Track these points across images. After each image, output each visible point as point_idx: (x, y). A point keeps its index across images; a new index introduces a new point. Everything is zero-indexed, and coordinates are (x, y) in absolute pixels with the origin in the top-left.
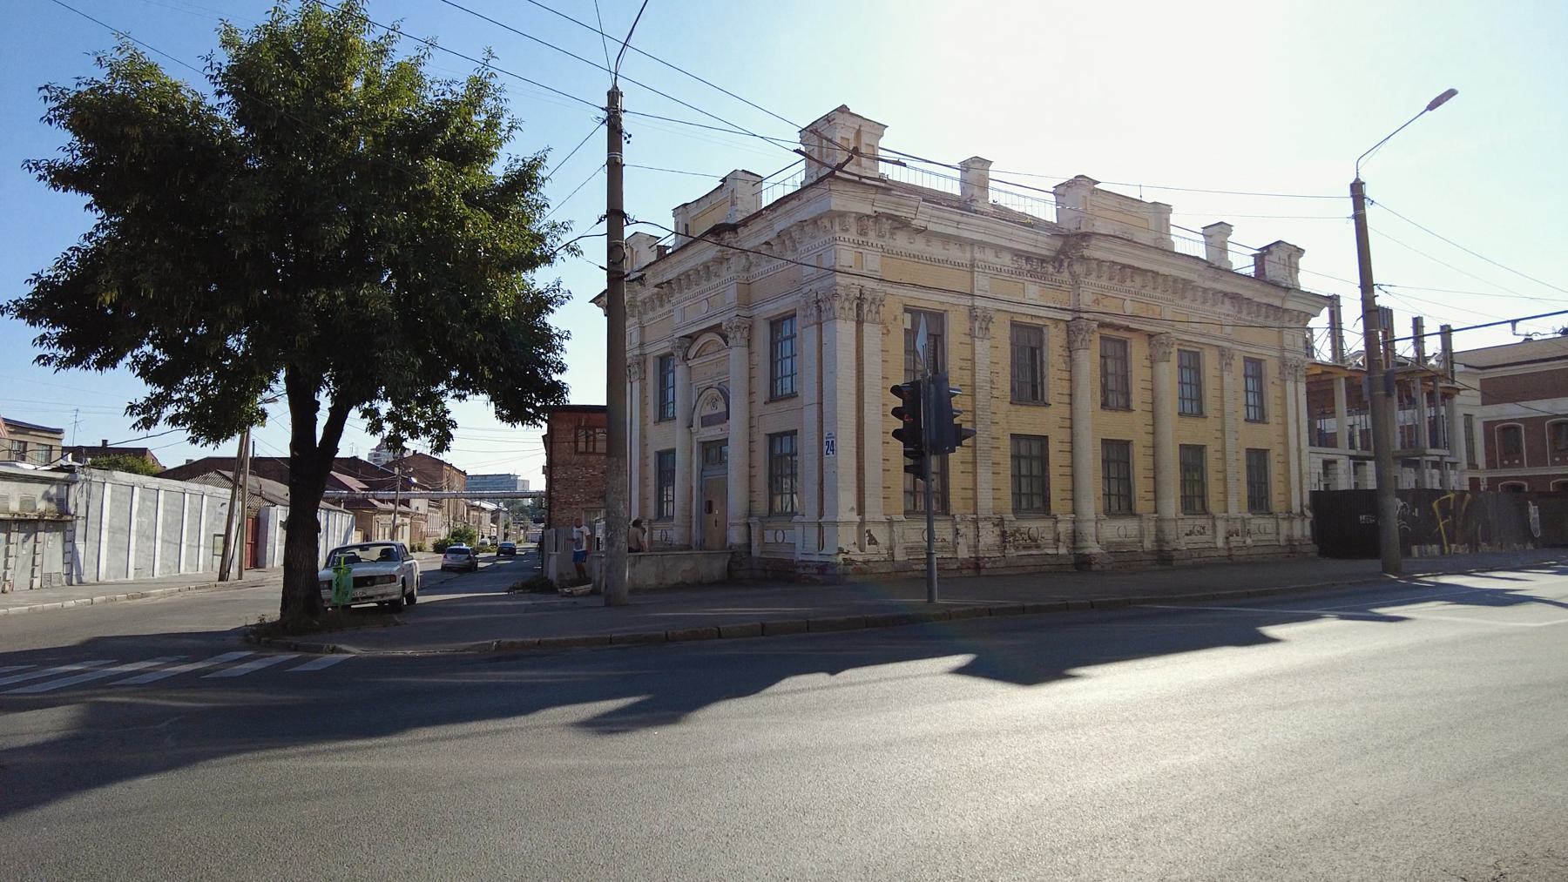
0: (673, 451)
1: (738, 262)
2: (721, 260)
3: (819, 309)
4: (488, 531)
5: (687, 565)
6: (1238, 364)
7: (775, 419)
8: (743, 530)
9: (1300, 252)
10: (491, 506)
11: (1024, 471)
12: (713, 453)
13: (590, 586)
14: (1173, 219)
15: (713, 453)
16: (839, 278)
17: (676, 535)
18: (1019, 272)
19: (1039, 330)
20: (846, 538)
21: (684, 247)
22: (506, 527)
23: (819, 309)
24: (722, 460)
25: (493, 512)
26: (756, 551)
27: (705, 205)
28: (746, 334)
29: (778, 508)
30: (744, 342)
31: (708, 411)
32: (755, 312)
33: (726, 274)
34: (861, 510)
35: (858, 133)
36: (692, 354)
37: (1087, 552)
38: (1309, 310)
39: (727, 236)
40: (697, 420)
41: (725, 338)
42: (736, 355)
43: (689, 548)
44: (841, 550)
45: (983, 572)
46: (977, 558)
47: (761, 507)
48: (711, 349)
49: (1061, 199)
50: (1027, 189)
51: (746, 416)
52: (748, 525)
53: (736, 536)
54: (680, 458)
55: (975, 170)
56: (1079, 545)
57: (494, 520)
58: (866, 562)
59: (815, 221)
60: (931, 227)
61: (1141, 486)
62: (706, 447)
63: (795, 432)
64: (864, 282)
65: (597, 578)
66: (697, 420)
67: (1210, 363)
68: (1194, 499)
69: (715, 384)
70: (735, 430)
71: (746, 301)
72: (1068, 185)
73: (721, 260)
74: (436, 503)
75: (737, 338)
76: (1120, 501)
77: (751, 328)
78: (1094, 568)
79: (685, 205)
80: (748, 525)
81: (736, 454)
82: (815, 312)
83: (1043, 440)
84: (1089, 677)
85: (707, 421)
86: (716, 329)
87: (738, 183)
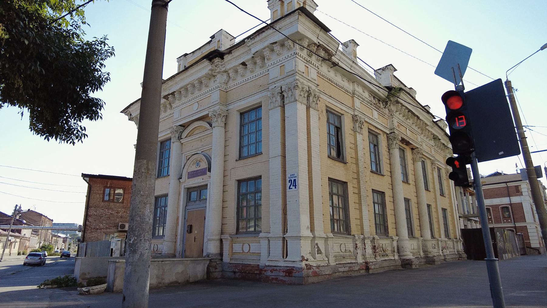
0: (166, 196)
1: (221, 78)
2: (211, 76)
3: (283, 97)
4: (59, 246)
5: (180, 268)
7: (247, 169)
8: (218, 243)
10: (64, 236)
12: (195, 195)
13: (104, 286)
15: (194, 195)
17: (165, 247)
20: (305, 248)
22: (70, 245)
23: (283, 97)
24: (201, 199)
25: (64, 238)
26: (226, 258)
28: (224, 120)
31: (194, 168)
32: (230, 107)
33: (212, 84)
36: (184, 135)
37: (408, 257)
39: (217, 60)
42: (218, 132)
43: (174, 256)
44: (303, 259)
45: (371, 272)
46: (367, 263)
47: (231, 227)
51: (222, 171)
52: (221, 241)
53: (212, 248)
54: (171, 201)
56: (402, 254)
57: (64, 241)
58: (318, 267)
60: (340, 64)
62: (189, 190)
65: (111, 279)
71: (225, 101)
73: (211, 76)
74: (35, 232)
75: (218, 123)
77: (227, 117)
78: (414, 267)
79: (186, 55)
80: (221, 241)
81: (213, 195)
82: (279, 98)
85: (193, 175)
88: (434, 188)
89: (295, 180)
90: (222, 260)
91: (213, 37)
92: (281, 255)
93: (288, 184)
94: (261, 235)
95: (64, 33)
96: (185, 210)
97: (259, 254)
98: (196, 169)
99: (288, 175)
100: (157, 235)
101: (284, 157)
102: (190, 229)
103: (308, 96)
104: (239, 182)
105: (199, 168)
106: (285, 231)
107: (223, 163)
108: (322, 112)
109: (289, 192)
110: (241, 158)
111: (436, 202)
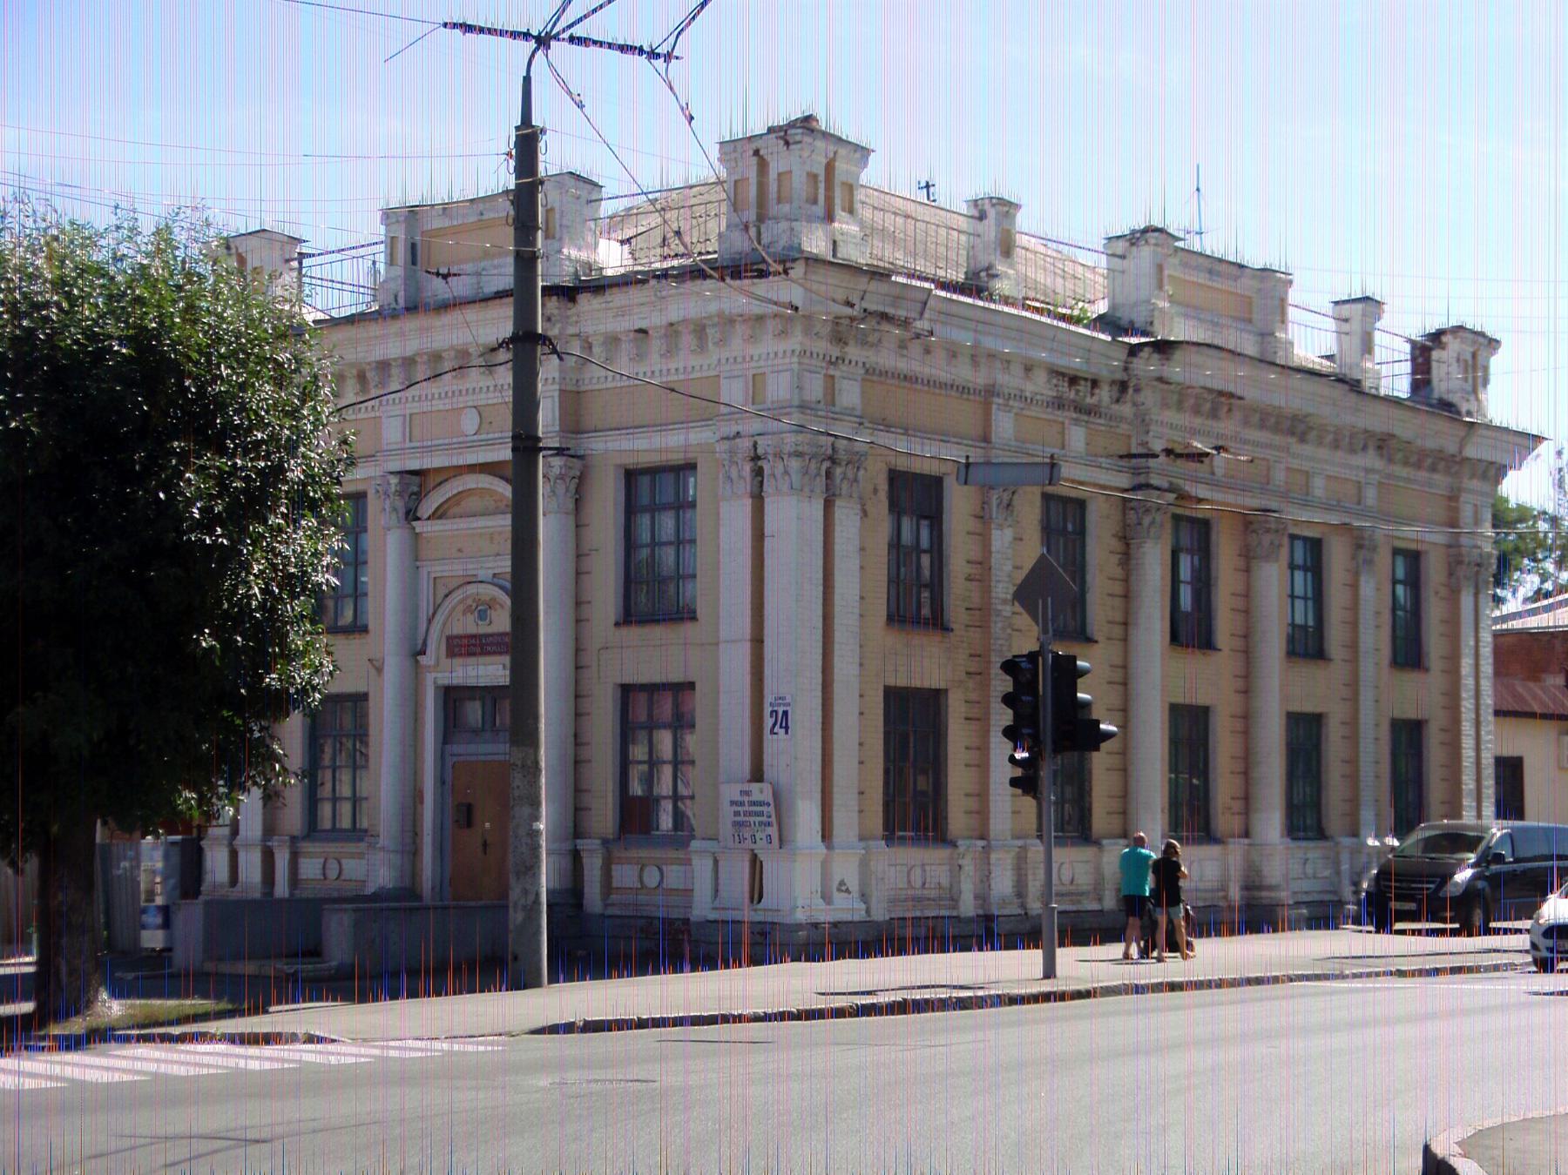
3: (759, 473)
6: (1383, 558)
7: (651, 655)
9: (1493, 344)
14: (1293, 296)
18: (1059, 404)
23: (759, 473)
29: (326, 824)
34: (234, 855)
38: (1498, 457)
40: (436, 646)
48: (472, 503)
50: (1069, 239)
55: (995, 212)
61: (1224, 788)
66: (436, 646)
67: (1337, 558)
72: (1137, 237)
88: (1353, 646)
89: (785, 713)
92: (747, 895)
93: (769, 722)
94: (695, 844)
96: (441, 757)
97: (688, 892)
98: (472, 630)
99: (769, 698)
100: (327, 825)
101: (758, 641)
102: (466, 815)
104: (627, 690)
105: (490, 630)
107: (573, 624)
108: (875, 491)
111: (1354, 699)
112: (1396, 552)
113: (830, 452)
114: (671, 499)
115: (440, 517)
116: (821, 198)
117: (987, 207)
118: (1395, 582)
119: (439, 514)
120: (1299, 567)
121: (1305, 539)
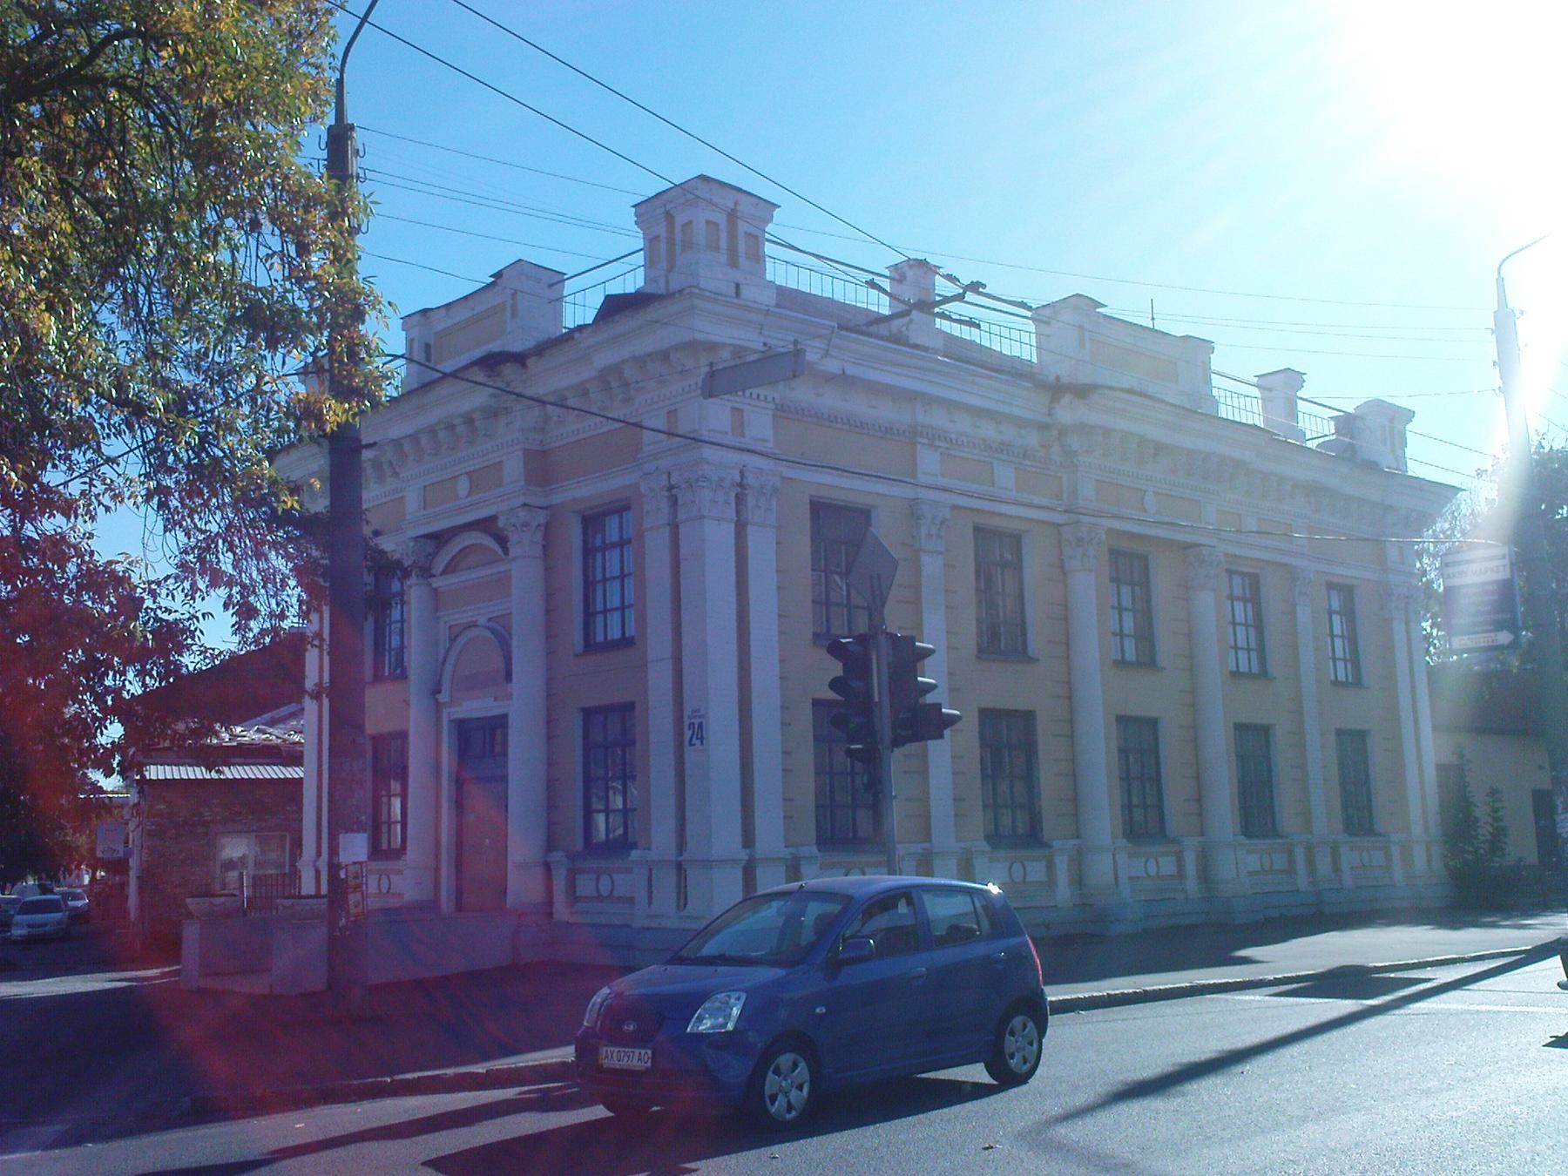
2: (492, 413)
3: (674, 501)
9: (1409, 415)
11: (1135, 801)
12: (479, 744)
14: (1217, 361)
16: (708, 452)
19: (1016, 540)
21: (425, 387)
23: (674, 501)
26: (561, 911)
27: (462, 315)
28: (539, 538)
30: (538, 551)
34: (748, 840)
35: (732, 215)
39: (509, 370)
41: (502, 541)
49: (1046, 330)
59: (664, 355)
62: (464, 729)
63: (630, 706)
64: (746, 457)
68: (1257, 812)
69: (482, 620)
70: (522, 705)
73: (492, 413)
76: (1144, 822)
79: (425, 311)
80: (548, 867)
82: (664, 505)
83: (1027, 717)
84: (691, 1171)
86: (485, 524)
87: (524, 285)
89: (700, 725)
90: (550, 914)
91: (498, 275)
93: (688, 733)
95: (171, 458)
99: (687, 712)
103: (740, 500)
104: (588, 713)
106: (681, 845)
109: (690, 756)
110: (590, 646)
112: (1330, 586)
113: (738, 479)
114: (615, 538)
115: (453, 571)
116: (723, 244)
117: (906, 269)
118: (1330, 613)
119: (449, 569)
120: (1238, 599)
121: (1243, 574)
